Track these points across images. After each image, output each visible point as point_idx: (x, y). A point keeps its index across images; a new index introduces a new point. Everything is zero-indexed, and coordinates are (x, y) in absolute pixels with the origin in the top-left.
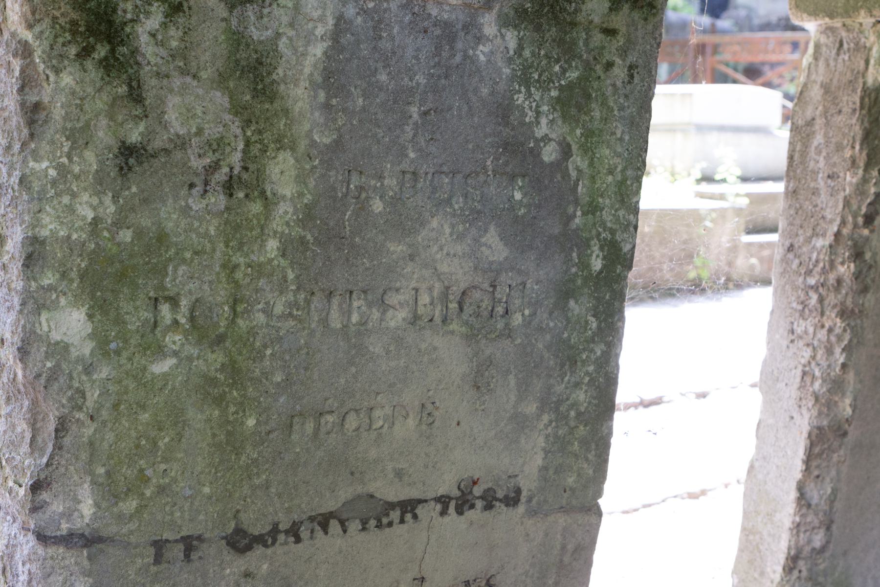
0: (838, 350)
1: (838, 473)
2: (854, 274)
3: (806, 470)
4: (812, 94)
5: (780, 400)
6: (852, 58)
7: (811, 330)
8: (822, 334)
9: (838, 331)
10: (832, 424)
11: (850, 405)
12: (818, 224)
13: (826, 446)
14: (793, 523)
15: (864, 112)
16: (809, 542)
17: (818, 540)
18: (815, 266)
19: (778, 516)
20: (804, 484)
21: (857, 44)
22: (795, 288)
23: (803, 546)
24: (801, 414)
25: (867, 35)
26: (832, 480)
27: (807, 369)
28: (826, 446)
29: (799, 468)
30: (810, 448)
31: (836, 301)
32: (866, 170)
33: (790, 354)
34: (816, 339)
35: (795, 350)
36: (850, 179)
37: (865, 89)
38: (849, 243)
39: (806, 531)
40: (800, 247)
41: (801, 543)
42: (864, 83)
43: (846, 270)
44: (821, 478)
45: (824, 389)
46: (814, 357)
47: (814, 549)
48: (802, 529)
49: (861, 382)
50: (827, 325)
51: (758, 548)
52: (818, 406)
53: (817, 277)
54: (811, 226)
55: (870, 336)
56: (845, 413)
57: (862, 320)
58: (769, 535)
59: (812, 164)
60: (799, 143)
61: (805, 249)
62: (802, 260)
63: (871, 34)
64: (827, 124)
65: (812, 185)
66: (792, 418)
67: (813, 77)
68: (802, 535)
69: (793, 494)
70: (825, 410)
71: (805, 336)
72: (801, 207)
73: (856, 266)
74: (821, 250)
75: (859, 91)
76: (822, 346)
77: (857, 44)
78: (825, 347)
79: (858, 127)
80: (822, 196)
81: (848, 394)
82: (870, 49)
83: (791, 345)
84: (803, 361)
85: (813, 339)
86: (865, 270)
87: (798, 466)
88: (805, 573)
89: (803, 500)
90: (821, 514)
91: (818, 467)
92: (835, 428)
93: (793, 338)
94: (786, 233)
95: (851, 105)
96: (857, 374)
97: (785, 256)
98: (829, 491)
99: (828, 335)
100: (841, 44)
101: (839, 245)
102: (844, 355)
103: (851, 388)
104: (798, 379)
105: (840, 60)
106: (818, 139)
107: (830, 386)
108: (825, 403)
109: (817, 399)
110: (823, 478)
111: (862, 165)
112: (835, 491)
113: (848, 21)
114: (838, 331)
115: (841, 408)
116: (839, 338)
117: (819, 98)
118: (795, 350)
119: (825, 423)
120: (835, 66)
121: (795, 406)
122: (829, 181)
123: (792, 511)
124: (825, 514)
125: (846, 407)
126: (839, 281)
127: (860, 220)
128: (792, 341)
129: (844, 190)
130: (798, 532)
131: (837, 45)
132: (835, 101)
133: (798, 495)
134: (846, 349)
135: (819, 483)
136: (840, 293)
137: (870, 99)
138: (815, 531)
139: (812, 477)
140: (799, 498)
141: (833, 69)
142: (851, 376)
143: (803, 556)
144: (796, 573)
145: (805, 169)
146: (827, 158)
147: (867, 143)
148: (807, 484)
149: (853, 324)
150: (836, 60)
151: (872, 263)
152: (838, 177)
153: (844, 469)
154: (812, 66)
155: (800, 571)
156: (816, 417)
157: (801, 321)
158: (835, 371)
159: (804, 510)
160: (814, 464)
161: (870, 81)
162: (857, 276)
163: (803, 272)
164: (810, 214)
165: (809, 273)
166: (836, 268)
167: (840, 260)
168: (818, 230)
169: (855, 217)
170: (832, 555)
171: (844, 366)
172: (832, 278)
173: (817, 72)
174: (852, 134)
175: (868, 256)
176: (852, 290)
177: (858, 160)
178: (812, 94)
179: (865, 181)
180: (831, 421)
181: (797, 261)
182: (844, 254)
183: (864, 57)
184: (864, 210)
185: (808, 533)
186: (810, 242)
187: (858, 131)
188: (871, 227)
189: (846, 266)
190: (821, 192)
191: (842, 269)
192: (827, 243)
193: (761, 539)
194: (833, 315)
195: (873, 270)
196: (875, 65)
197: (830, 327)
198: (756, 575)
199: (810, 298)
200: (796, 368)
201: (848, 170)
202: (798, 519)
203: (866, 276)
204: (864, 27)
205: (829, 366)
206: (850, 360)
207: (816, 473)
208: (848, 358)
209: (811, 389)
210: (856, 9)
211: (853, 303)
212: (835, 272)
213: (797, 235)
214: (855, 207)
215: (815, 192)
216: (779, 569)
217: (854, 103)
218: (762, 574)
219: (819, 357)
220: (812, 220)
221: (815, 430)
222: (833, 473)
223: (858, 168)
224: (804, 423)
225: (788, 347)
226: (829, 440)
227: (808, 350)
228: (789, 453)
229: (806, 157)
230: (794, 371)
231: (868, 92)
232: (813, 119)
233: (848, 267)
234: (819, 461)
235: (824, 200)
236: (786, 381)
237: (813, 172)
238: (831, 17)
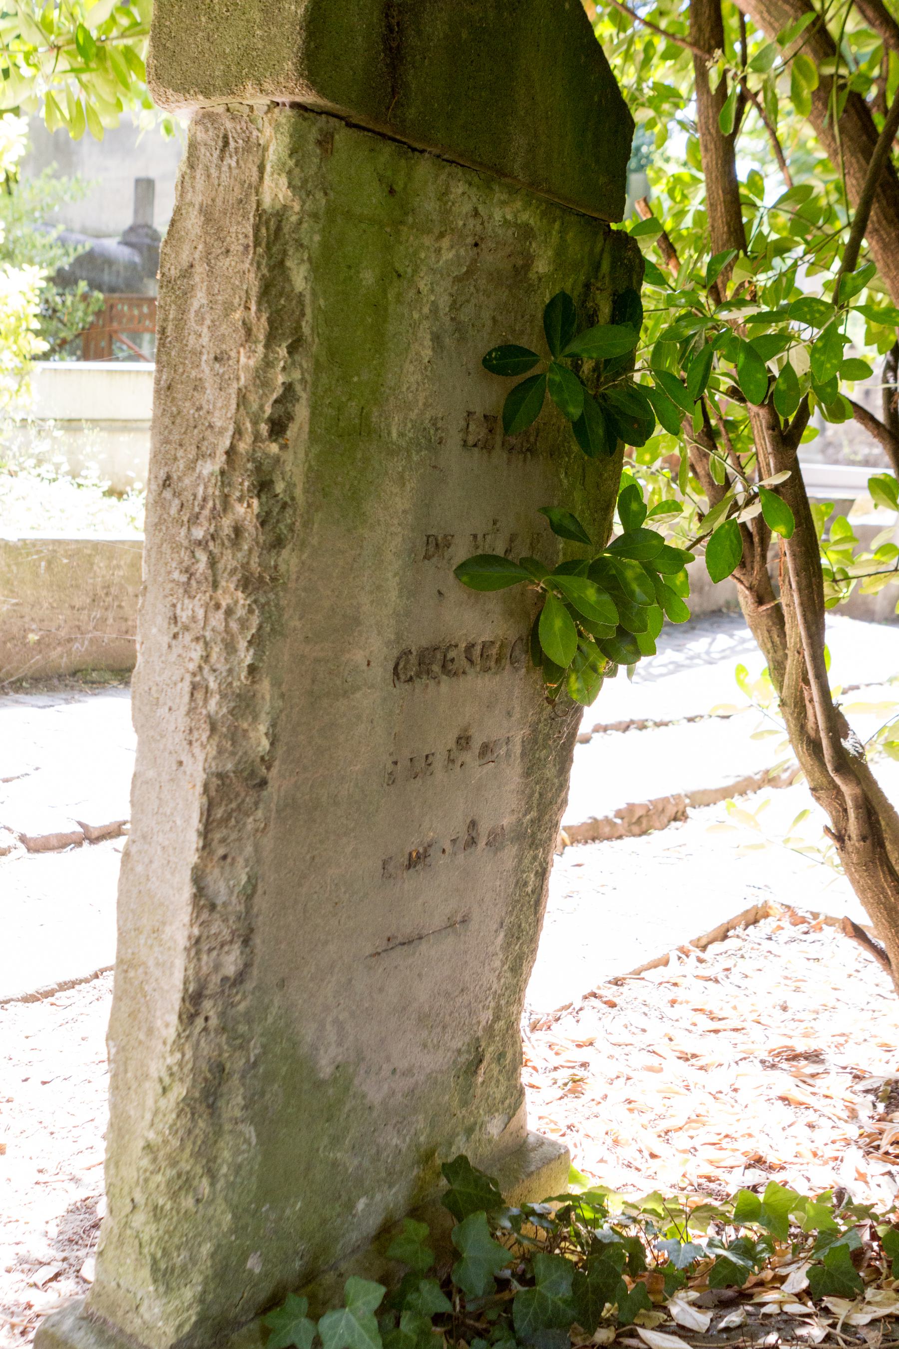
0: (242, 644)
1: (257, 848)
2: (258, 516)
3: (204, 847)
4: (189, 224)
5: (162, 736)
6: (241, 162)
7: (200, 613)
8: (217, 619)
9: (240, 612)
10: (241, 767)
11: (266, 734)
12: (204, 439)
13: (234, 805)
14: (190, 938)
15: (260, 250)
16: (217, 967)
17: (231, 964)
18: (202, 508)
19: (168, 930)
20: (203, 871)
21: (247, 141)
22: (176, 547)
23: (208, 975)
24: (193, 755)
25: (260, 126)
26: (247, 861)
27: (198, 678)
28: (234, 805)
29: (194, 846)
30: (209, 810)
31: (235, 563)
32: (267, 346)
33: (173, 657)
34: (209, 628)
35: (180, 651)
36: (247, 360)
37: (260, 213)
38: (250, 466)
39: (210, 950)
40: (180, 479)
41: (205, 970)
42: (259, 203)
43: (246, 511)
44: (229, 860)
45: (225, 710)
46: (206, 658)
47: (225, 979)
48: (205, 947)
49: (282, 696)
50: (224, 604)
51: (142, 989)
52: (216, 738)
53: (206, 524)
54: (194, 442)
55: (296, 623)
56: (260, 749)
57: (277, 594)
58: (157, 964)
59: (192, 339)
60: (173, 307)
61: (187, 481)
62: (183, 498)
63: (267, 124)
64: (211, 272)
65: (193, 374)
66: (181, 763)
67: (189, 196)
68: (205, 957)
69: (188, 890)
70: (228, 745)
71: (193, 625)
72: (179, 413)
73: (261, 504)
74: (209, 481)
75: (251, 216)
76: (219, 639)
77: (247, 141)
78: (223, 640)
79: (252, 275)
80: (208, 392)
81: (263, 716)
82: (265, 149)
83: (174, 642)
84: (192, 666)
85: (204, 628)
86: (276, 510)
87: (193, 841)
88: (214, 1022)
89: (203, 899)
90: (232, 919)
91: (223, 840)
92: (245, 774)
93: (176, 630)
94: (160, 457)
95: (242, 241)
96: (276, 683)
97: (160, 494)
98: (244, 879)
99: (226, 619)
100: (226, 144)
101: (234, 470)
102: (252, 652)
103: (267, 708)
104: (187, 698)
105: (225, 169)
106: (200, 298)
107: (232, 704)
108: (227, 733)
109: (213, 729)
110: (233, 859)
111: (262, 337)
112: (253, 881)
113: (233, 102)
114: (240, 612)
115: (253, 741)
116: (244, 624)
117: (198, 230)
118: (180, 651)
119: (229, 766)
120: (219, 178)
121: (185, 743)
122: (217, 365)
123: (186, 919)
124: (239, 918)
125: (259, 739)
126: (238, 530)
127: (264, 428)
128: (175, 636)
129: (238, 379)
130: (198, 952)
131: (220, 144)
132: (220, 234)
133: (194, 890)
134: (256, 642)
135: (227, 868)
136: (240, 550)
137: (267, 229)
138: (226, 948)
139: (216, 858)
140: (195, 896)
141: (216, 183)
142: (265, 686)
143: (207, 992)
144: (200, 1022)
145: (182, 350)
146: (213, 328)
147: (268, 302)
148: (208, 870)
149: (262, 600)
150: (219, 167)
151: (288, 499)
152: (229, 358)
153: (268, 842)
154: (187, 178)
155: (206, 1019)
156: (214, 758)
157: (186, 601)
158: (239, 680)
159: (205, 916)
160: (217, 836)
161: (267, 201)
162: (264, 521)
163: (185, 519)
164: (192, 423)
165: (194, 519)
166: (233, 507)
167: (238, 494)
168: (204, 449)
169: (255, 423)
170: (258, 988)
171: (252, 669)
172: (227, 523)
173: (193, 187)
174: (245, 287)
175: (279, 487)
176: (257, 543)
177: (255, 330)
178: (189, 224)
179: (268, 364)
180: (239, 762)
181: (177, 502)
182: (241, 484)
183: (258, 162)
184: (268, 410)
185: (215, 953)
186: (194, 469)
187: (253, 282)
188: (281, 441)
189: (245, 505)
190: (207, 385)
191: (240, 509)
192: (217, 468)
193: (146, 973)
194: (232, 586)
195: (289, 511)
196: (272, 174)
197: (228, 606)
198: (142, 1036)
199: (197, 562)
200: (182, 679)
201: (242, 345)
202: (196, 931)
203: (278, 521)
204: (256, 112)
205: (230, 671)
206: (261, 660)
207: (221, 851)
208: (258, 656)
209: (204, 712)
210: (240, 80)
211: (260, 565)
212: (230, 515)
213: (175, 459)
214: (255, 407)
215: (198, 386)
216: (174, 1019)
217: (246, 236)
218: (150, 1032)
219: (214, 657)
220: (196, 431)
221: (214, 779)
222: (249, 849)
223: (256, 342)
224: (196, 769)
225: (170, 647)
226: (237, 795)
227: (198, 648)
228: (179, 822)
229: (183, 329)
230: (180, 685)
231: (264, 218)
232: (192, 266)
233: (249, 506)
234: (225, 832)
235: (211, 397)
236: (169, 704)
237: (193, 352)
238: (207, 94)
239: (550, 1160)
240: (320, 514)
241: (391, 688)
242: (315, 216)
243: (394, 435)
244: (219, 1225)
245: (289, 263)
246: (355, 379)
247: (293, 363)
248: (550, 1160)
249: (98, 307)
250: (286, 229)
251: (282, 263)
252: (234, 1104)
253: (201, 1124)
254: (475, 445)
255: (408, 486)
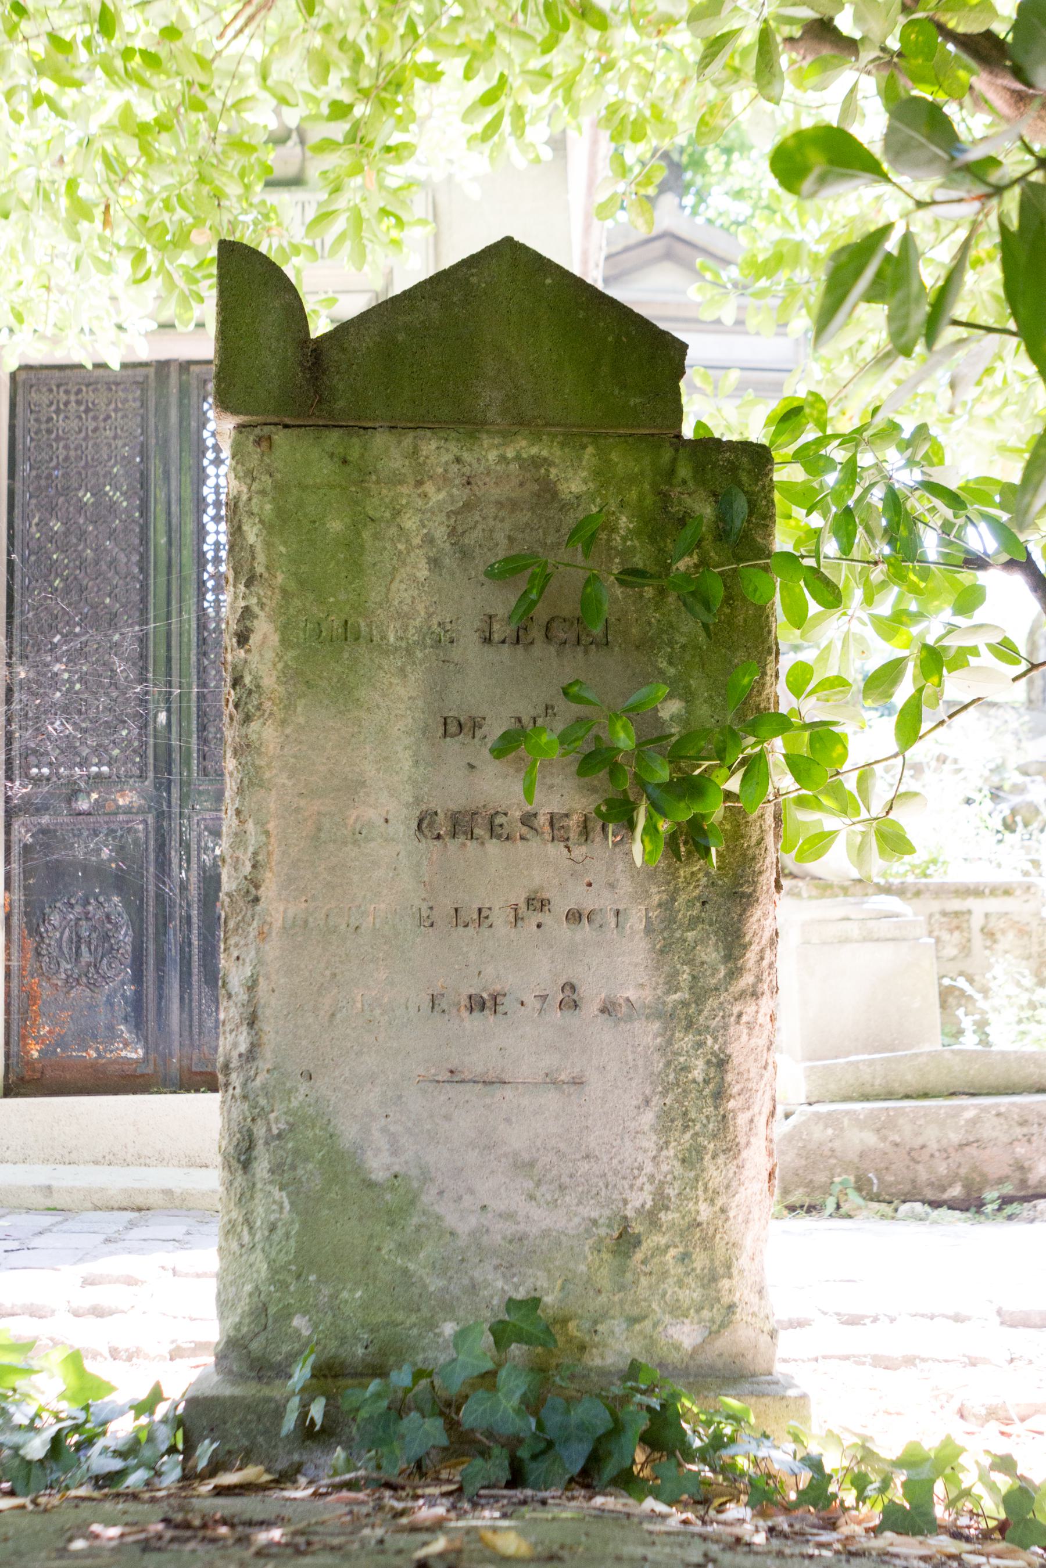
16: (235, 1045)
39: (232, 1031)
47: (240, 1055)
91: (236, 945)
175: (247, 680)
207: (235, 954)
234: (237, 938)
239: (742, 1376)
240: (303, 701)
241: (416, 842)
242: (263, 492)
243: (392, 639)
244: (258, 1272)
245: (245, 528)
246: (332, 600)
247: (251, 593)
248: (742, 1376)
249: (979, 719)
250: (241, 504)
251: (240, 528)
252: (262, 1167)
253: (239, 1179)
254: (503, 642)
255: (412, 678)
